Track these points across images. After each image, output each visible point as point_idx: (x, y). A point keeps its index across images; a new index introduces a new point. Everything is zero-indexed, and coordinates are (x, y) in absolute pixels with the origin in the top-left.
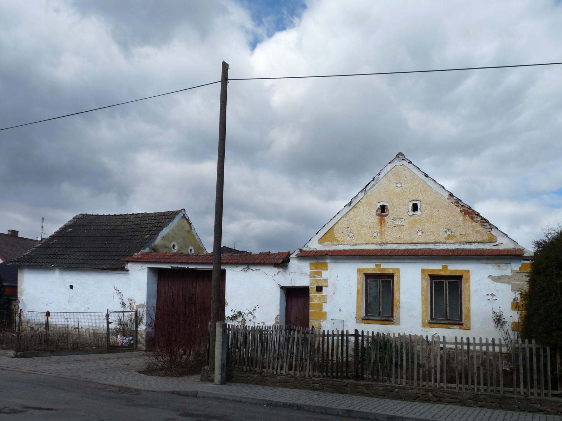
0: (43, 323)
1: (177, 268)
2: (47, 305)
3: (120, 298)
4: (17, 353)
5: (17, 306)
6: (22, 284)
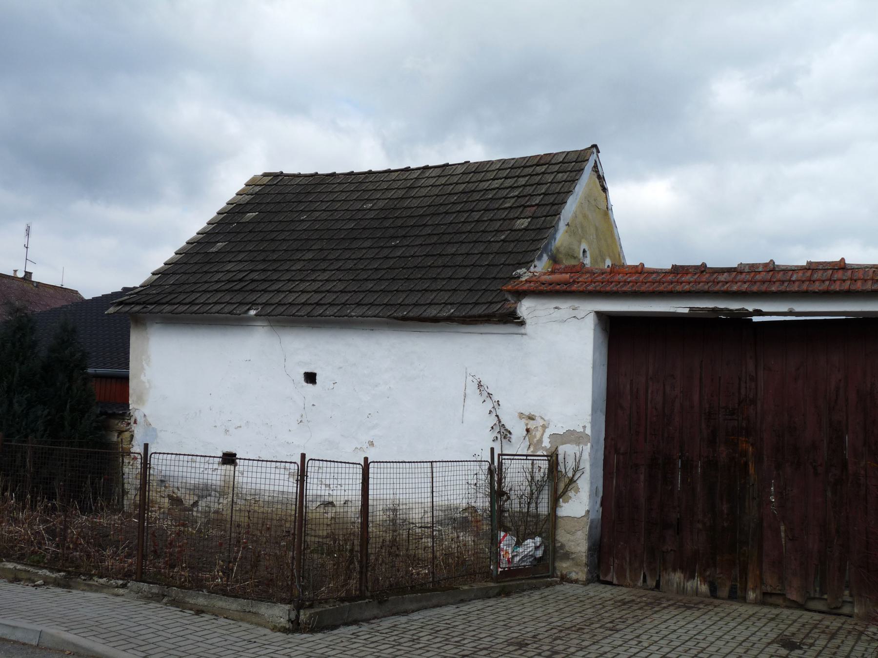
0: (214, 487)
1: (713, 316)
2: (227, 431)
3: (490, 412)
4: (298, 612)
5: (127, 435)
6: (143, 368)
